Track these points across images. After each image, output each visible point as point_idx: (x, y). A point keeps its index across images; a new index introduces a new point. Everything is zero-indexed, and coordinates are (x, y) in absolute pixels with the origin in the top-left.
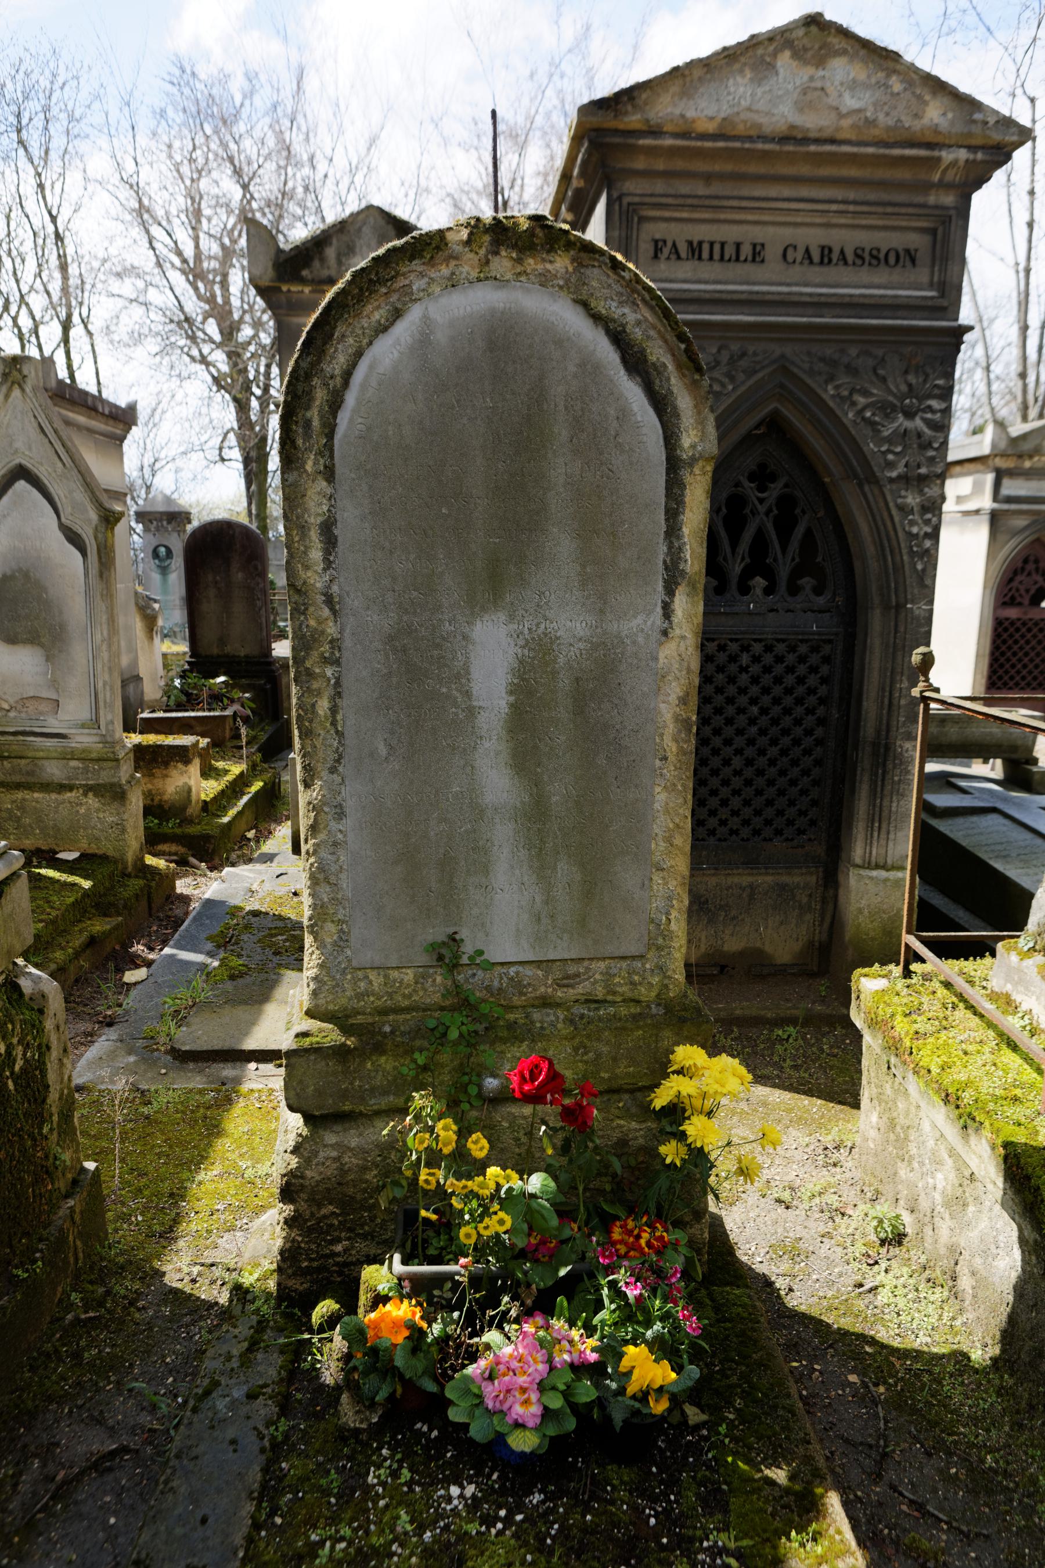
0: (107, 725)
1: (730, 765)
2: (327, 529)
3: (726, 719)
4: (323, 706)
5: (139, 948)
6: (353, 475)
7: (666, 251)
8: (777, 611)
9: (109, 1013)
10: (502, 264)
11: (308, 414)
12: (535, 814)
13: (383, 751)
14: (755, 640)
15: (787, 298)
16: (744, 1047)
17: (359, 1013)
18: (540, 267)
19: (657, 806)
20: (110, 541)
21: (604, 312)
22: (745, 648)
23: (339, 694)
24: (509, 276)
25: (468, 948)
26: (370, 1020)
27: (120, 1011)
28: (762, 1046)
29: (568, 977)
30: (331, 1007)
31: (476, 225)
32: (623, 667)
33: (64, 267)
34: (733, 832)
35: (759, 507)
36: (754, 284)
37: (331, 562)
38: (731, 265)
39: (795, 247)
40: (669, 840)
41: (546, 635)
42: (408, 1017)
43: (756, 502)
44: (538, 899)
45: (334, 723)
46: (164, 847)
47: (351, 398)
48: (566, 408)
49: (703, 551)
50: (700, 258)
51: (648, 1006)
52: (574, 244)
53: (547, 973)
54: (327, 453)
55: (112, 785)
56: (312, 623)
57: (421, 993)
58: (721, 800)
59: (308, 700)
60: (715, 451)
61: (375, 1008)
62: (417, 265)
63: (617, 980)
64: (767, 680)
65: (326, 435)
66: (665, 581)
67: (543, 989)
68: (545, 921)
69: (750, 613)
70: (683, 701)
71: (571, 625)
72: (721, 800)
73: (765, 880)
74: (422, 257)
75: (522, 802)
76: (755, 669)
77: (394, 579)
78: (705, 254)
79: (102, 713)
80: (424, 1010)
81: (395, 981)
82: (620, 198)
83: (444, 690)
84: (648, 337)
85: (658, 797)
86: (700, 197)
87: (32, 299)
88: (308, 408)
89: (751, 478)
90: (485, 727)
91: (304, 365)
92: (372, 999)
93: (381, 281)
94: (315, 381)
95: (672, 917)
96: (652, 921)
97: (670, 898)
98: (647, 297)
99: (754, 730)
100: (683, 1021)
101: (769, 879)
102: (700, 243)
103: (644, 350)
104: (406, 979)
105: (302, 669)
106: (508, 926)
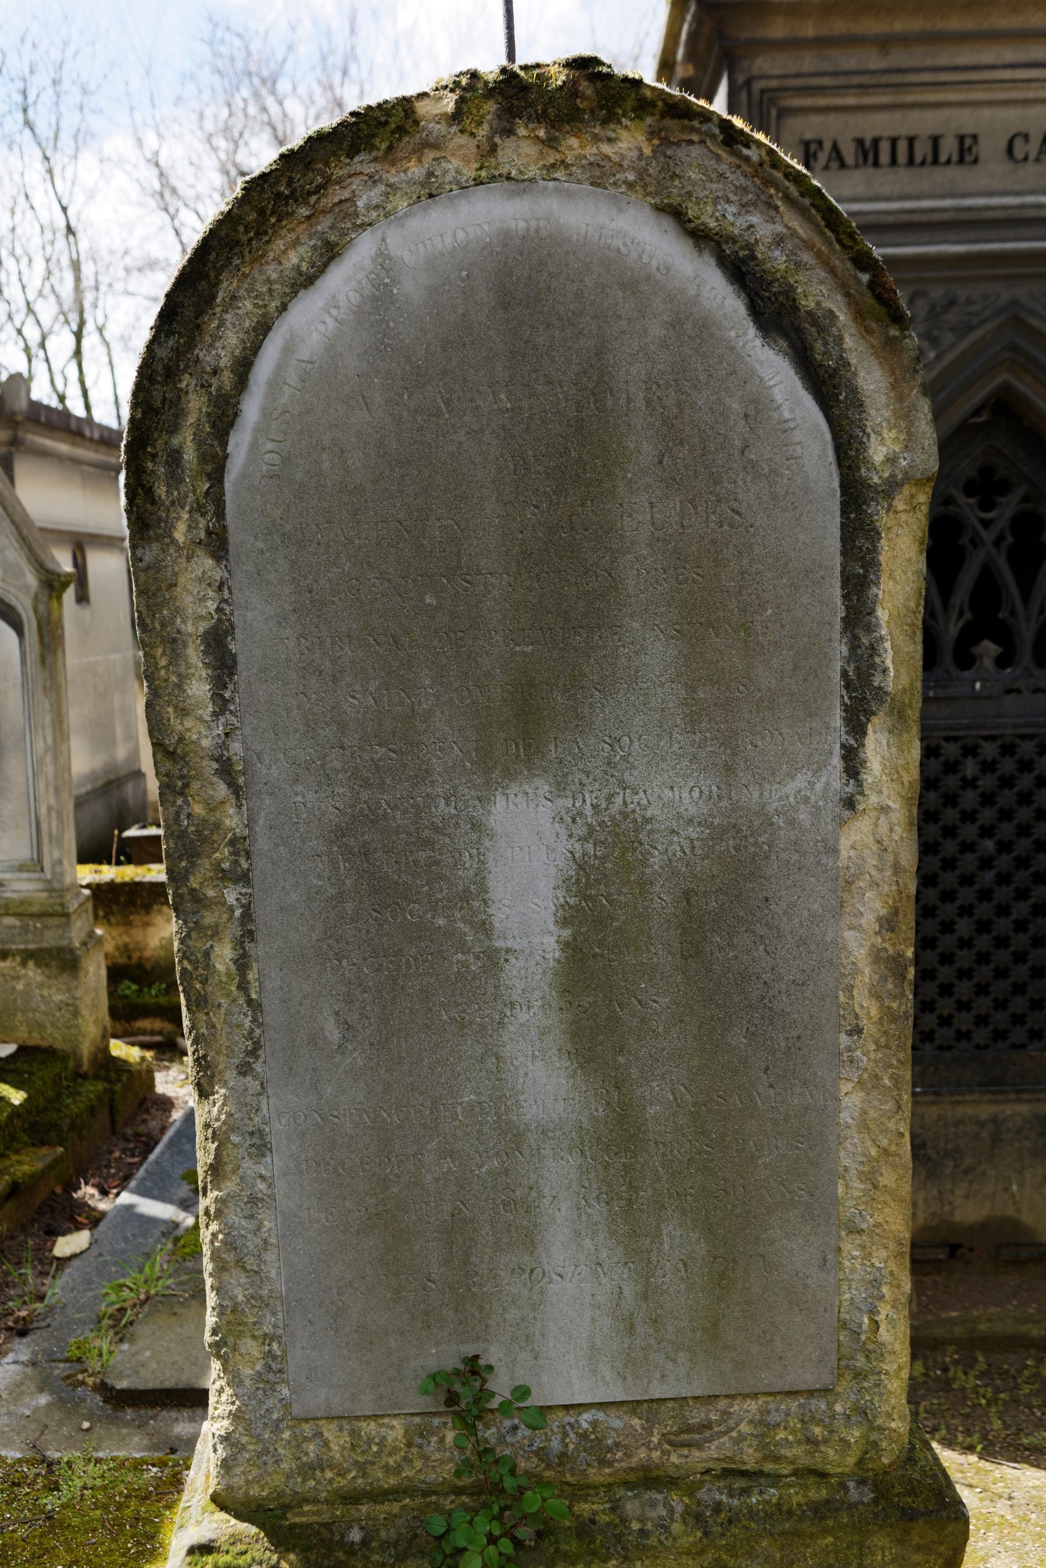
0: (53, 865)
1: (952, 931)
2: (218, 643)
3: (944, 860)
4: (224, 955)
5: (88, 1192)
6: (261, 545)
7: (823, 157)
8: (1018, 691)
9: (23, 1313)
10: (520, 152)
11: (175, 441)
12: (617, 1140)
13: (333, 1033)
14: (986, 738)
15: (1017, 214)
16: (997, 1390)
17: (307, 1501)
18: (590, 151)
19: (845, 1117)
20: (55, 614)
21: (712, 224)
22: (970, 751)
23: (250, 935)
24: (533, 171)
25: (501, 1386)
26: (326, 1517)
27: (39, 1306)
28: (1026, 1389)
29: (689, 1429)
30: (255, 1491)
31: (470, 87)
32: (772, 868)
33: (76, 266)
34: (963, 1035)
35: (984, 533)
36: (963, 195)
37: (226, 702)
38: (926, 170)
39: (1026, 137)
40: (870, 1178)
41: (625, 815)
42: (395, 1508)
43: (979, 527)
44: (627, 1291)
45: (243, 986)
46: (145, 1024)
47: (252, 408)
48: (648, 403)
49: (916, 650)
50: (876, 164)
51: (843, 1486)
52: (652, 104)
53: (650, 1423)
54: (211, 508)
55: (61, 950)
56: (198, 809)
57: (418, 1464)
58: (941, 986)
59: (199, 945)
60: (934, 466)
61: (336, 1492)
62: (363, 163)
63: (781, 1435)
64: (1007, 798)
65: (209, 476)
66: (846, 708)
67: (642, 1453)
68: (641, 1329)
69: (976, 697)
70: (888, 924)
71: (672, 797)
72: (941, 986)
73: (1016, 1110)
74: (372, 147)
75: (592, 1118)
76: (987, 782)
77: (342, 727)
78: (885, 157)
79: (46, 849)
80: (425, 1494)
81: (370, 1441)
82: (748, 83)
83: (441, 922)
84: (799, 265)
85: (846, 1101)
86: (873, 73)
87: (39, 306)
88: (174, 429)
89: (969, 489)
90: (520, 985)
91: (162, 353)
92: (329, 1475)
93: (300, 197)
94: (186, 381)
95: (881, 1317)
96: (844, 1325)
97: (876, 1283)
98: (794, 190)
99: (989, 876)
100: (909, 1515)
101: (1023, 1109)
102: (876, 141)
103: (792, 289)
104: (391, 1436)
105: (183, 890)
106: (575, 1340)
